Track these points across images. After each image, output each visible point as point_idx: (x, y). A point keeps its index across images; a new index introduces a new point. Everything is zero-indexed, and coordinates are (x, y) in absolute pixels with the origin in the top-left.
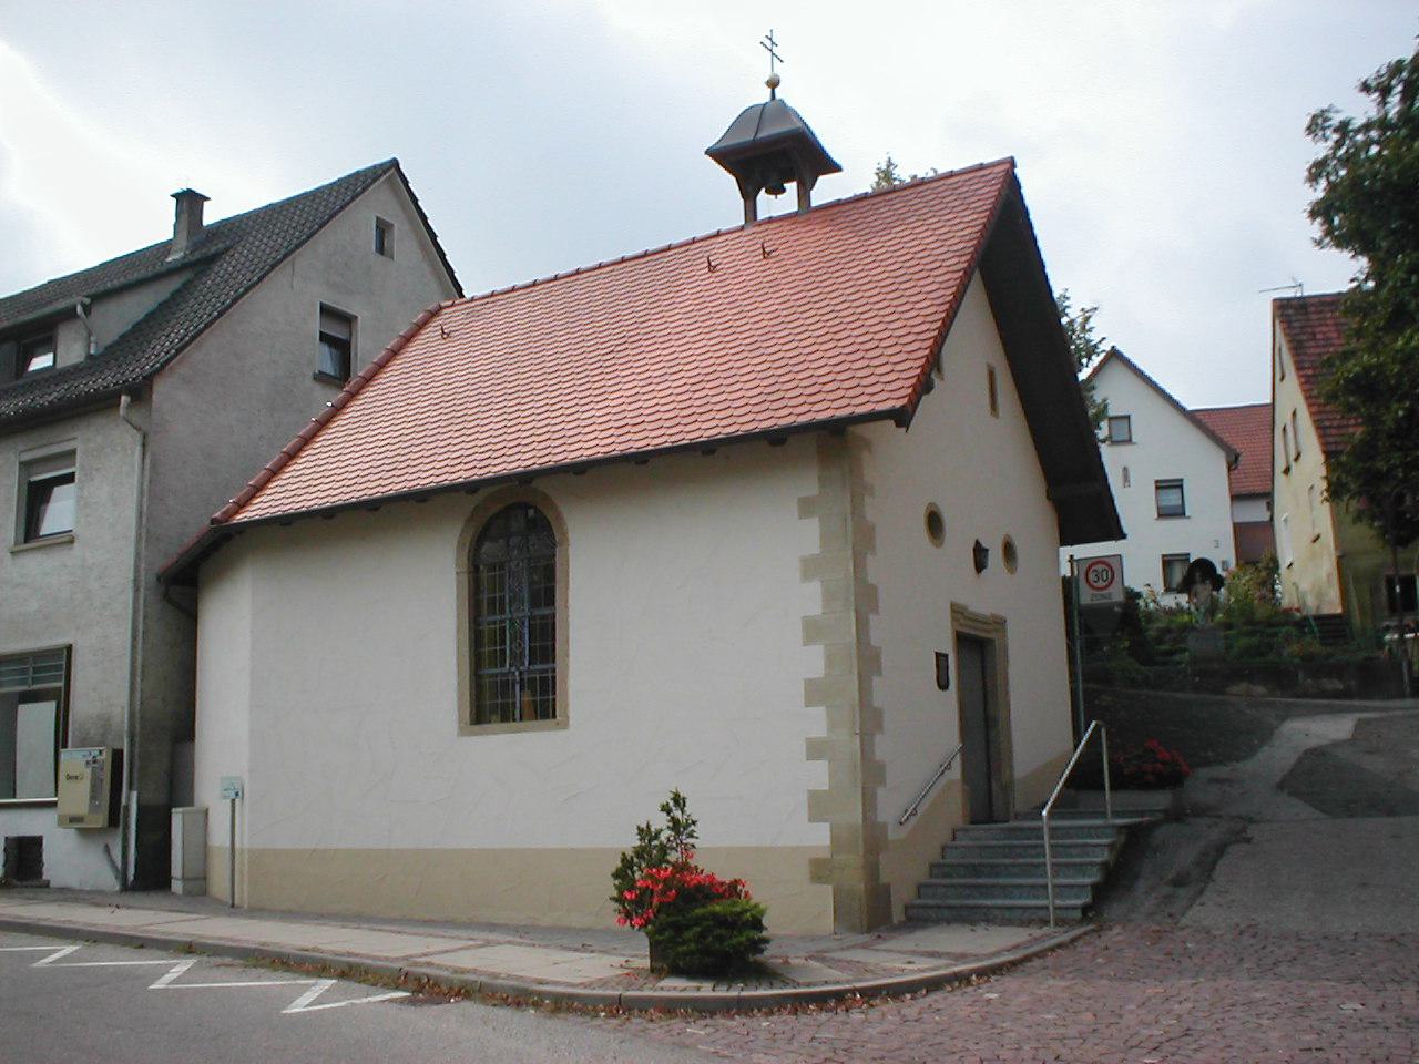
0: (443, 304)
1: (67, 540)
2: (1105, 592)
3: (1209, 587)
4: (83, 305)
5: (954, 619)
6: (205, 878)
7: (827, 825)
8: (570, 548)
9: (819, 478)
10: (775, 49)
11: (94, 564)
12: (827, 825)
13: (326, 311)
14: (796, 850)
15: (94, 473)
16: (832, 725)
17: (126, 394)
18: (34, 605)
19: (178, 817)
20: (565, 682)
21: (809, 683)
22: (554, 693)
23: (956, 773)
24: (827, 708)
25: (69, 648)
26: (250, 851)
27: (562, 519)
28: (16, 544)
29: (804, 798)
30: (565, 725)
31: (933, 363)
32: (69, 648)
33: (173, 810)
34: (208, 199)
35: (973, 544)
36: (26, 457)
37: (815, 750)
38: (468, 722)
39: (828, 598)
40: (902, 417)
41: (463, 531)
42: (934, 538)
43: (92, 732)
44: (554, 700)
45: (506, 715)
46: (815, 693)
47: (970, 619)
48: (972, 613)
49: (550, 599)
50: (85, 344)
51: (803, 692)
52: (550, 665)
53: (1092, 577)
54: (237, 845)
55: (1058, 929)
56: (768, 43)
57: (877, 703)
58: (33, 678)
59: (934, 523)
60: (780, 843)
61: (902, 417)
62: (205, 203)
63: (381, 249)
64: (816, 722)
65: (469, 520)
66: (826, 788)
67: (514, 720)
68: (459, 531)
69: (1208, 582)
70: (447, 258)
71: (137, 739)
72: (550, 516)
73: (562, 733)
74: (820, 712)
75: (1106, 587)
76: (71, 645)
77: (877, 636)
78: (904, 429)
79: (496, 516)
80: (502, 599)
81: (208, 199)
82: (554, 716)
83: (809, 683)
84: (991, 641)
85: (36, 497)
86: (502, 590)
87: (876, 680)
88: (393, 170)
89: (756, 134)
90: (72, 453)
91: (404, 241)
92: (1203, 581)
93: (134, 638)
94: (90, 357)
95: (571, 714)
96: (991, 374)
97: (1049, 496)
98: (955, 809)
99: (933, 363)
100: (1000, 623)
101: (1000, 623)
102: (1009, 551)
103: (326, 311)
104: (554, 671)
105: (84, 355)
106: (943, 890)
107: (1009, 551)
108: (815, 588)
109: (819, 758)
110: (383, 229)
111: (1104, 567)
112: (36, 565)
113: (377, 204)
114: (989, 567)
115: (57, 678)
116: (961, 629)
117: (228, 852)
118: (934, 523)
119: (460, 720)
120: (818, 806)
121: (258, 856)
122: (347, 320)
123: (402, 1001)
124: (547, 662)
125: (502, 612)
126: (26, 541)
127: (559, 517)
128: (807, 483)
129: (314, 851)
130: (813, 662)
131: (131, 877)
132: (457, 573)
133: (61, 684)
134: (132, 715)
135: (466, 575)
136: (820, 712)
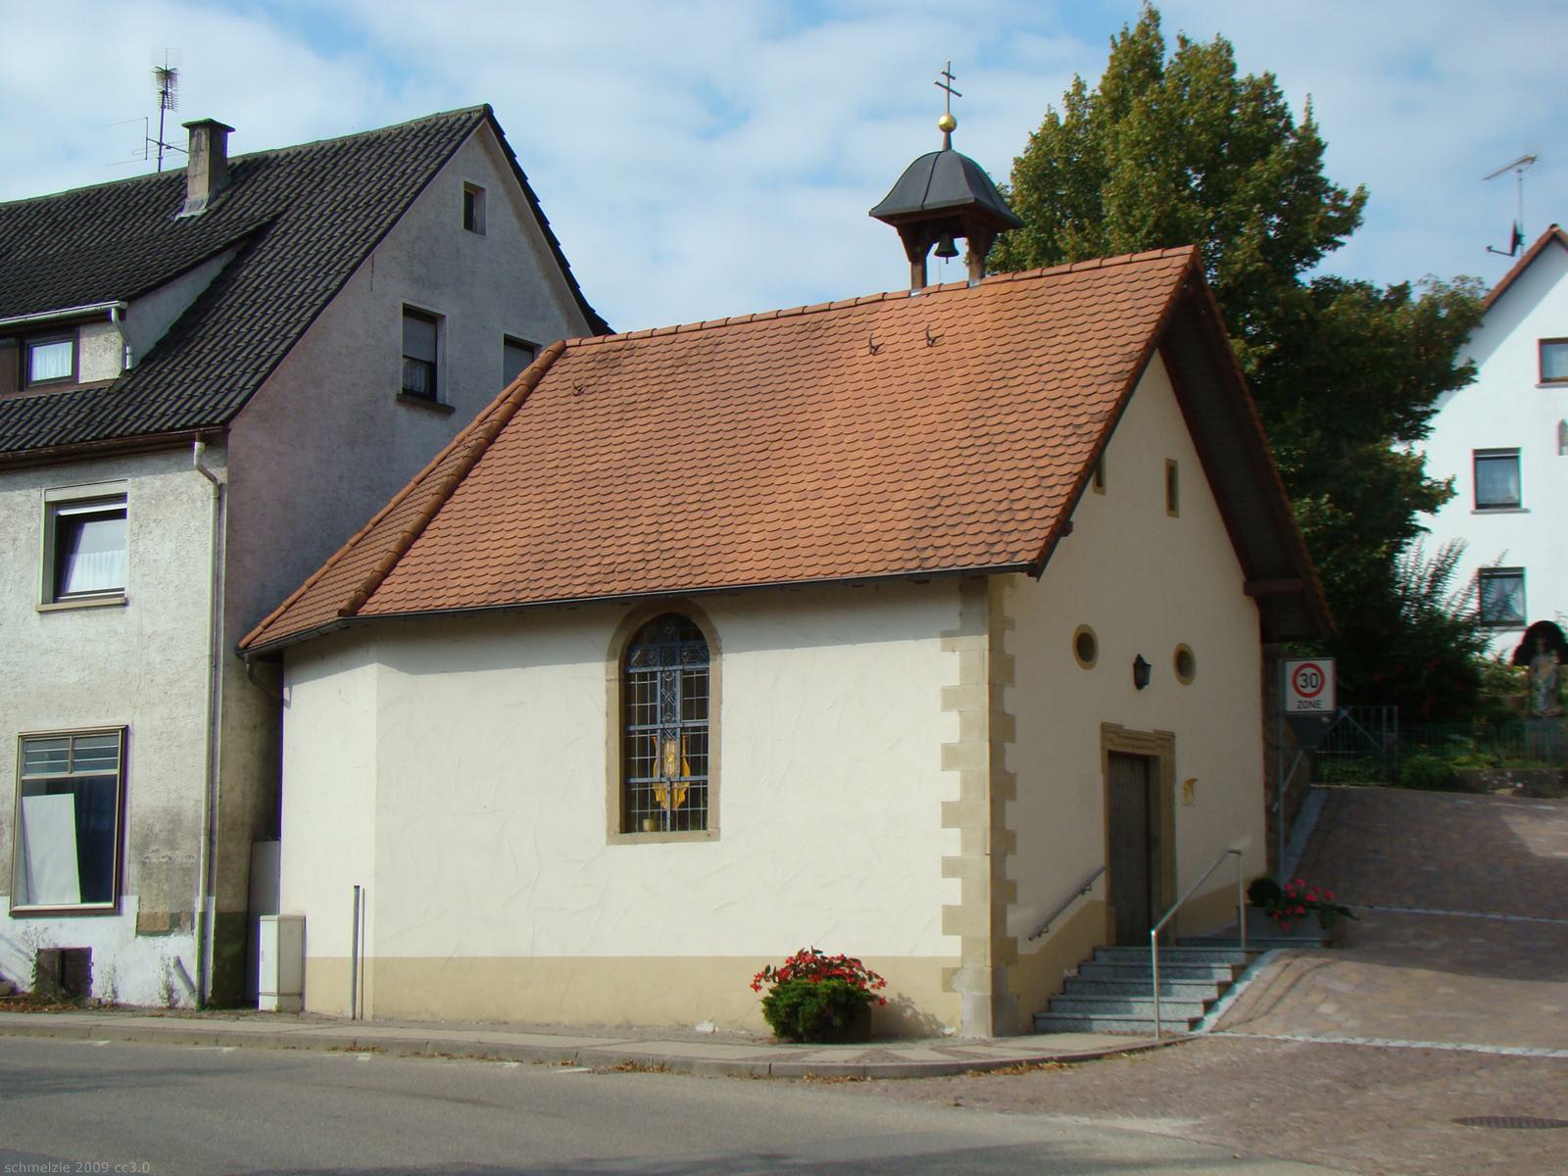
0: (568, 344)
1: (115, 600)
2: (1311, 699)
3: (1555, 660)
4: (118, 309)
5: (1103, 738)
6: (301, 995)
7: (959, 937)
8: (724, 663)
9: (961, 614)
10: (953, 85)
11: (154, 632)
12: (959, 937)
13: (410, 312)
14: (931, 959)
15: (153, 525)
16: (966, 847)
17: (201, 440)
18: (72, 677)
19: (268, 931)
20: (717, 793)
21: (946, 806)
22: (706, 805)
23: (1099, 891)
24: (962, 829)
25: (126, 731)
26: (376, 959)
27: (716, 633)
28: (44, 602)
29: (939, 912)
30: (715, 837)
31: (1093, 470)
32: (126, 731)
33: (262, 918)
34: (232, 130)
35: (1133, 660)
36: (56, 496)
37: (950, 868)
38: (618, 830)
39: (966, 727)
40: (1035, 569)
41: (614, 638)
42: (1084, 660)
43: (157, 828)
44: (705, 812)
45: (684, 827)
46: (951, 814)
47: (1127, 738)
48: (1130, 732)
49: (702, 711)
50: (120, 355)
51: (574, 951)
52: (701, 778)
53: (1300, 681)
54: (359, 955)
55: (657, 772)
56: (944, 80)
57: (1009, 826)
58: (73, 763)
59: (1085, 647)
60: (917, 954)
61: (1035, 569)
62: (229, 134)
63: (469, 223)
64: (952, 842)
65: (620, 628)
66: (960, 903)
67: (665, 830)
68: (611, 635)
69: (1554, 652)
70: (529, 182)
71: (216, 839)
72: (704, 630)
73: (714, 844)
74: (955, 833)
75: (1314, 694)
76: (127, 726)
77: (1010, 764)
78: (1035, 579)
79: (647, 625)
80: (654, 708)
81: (232, 130)
82: (705, 828)
83: (946, 806)
84: (1156, 758)
85: (64, 537)
86: (654, 699)
87: (1009, 804)
88: (485, 120)
89: (924, 201)
90: (122, 497)
91: (498, 211)
92: (1547, 651)
93: (212, 723)
94: (124, 372)
95: (723, 824)
96: (1172, 472)
97: (1248, 590)
98: (1099, 929)
99: (1093, 470)
100: (1167, 739)
101: (1167, 739)
102: (1184, 662)
103: (410, 312)
104: (705, 782)
105: (119, 371)
106: (1072, 1004)
107: (1184, 662)
108: (953, 718)
109: (954, 875)
110: (472, 195)
111: (1314, 671)
112: (69, 626)
113: (470, 164)
114: (1150, 683)
115: (113, 765)
116: (1113, 748)
117: (350, 963)
118: (1085, 647)
119: (609, 831)
120: (952, 920)
121: (383, 965)
122: (433, 319)
123: (589, 1072)
124: (699, 774)
125: (653, 721)
126: (55, 601)
127: (713, 631)
128: (950, 613)
129: (450, 958)
130: (950, 786)
131: (209, 994)
132: (607, 681)
133: (116, 772)
134: (211, 809)
135: (617, 683)
136: (955, 833)
